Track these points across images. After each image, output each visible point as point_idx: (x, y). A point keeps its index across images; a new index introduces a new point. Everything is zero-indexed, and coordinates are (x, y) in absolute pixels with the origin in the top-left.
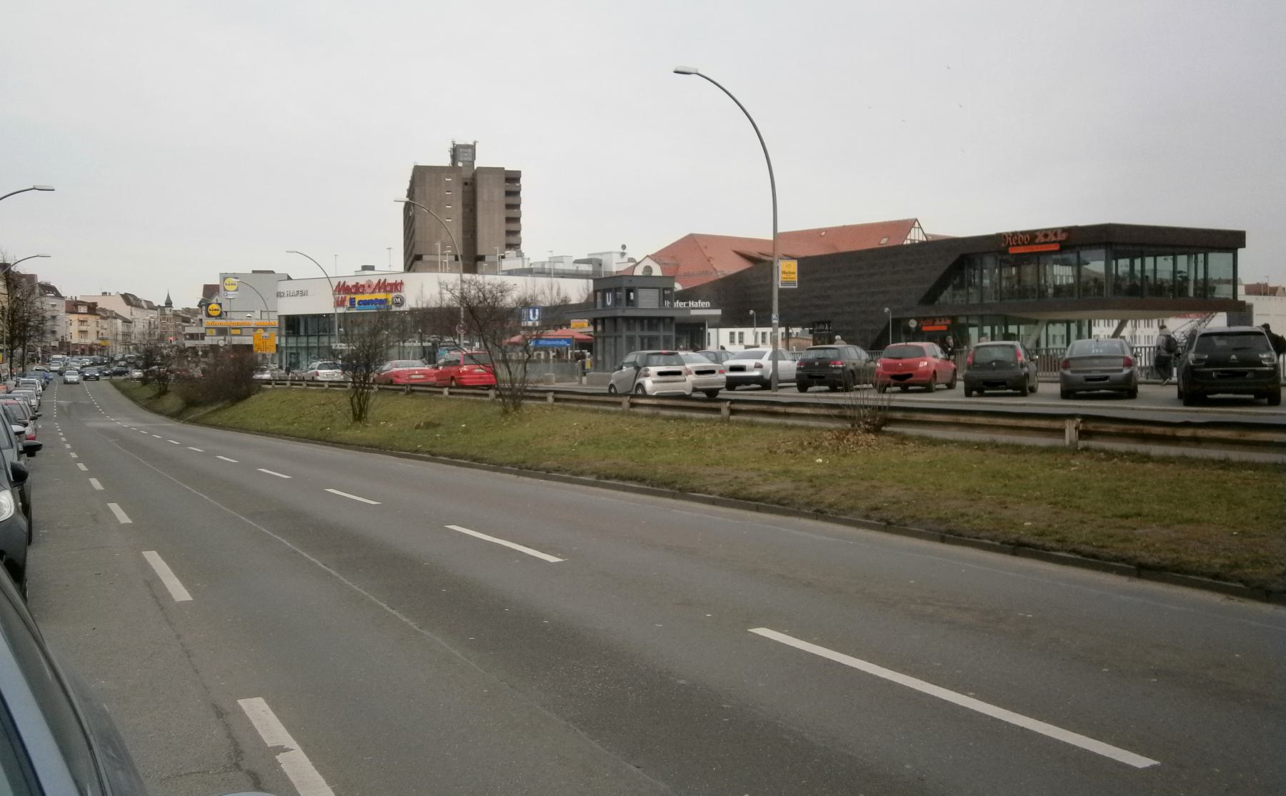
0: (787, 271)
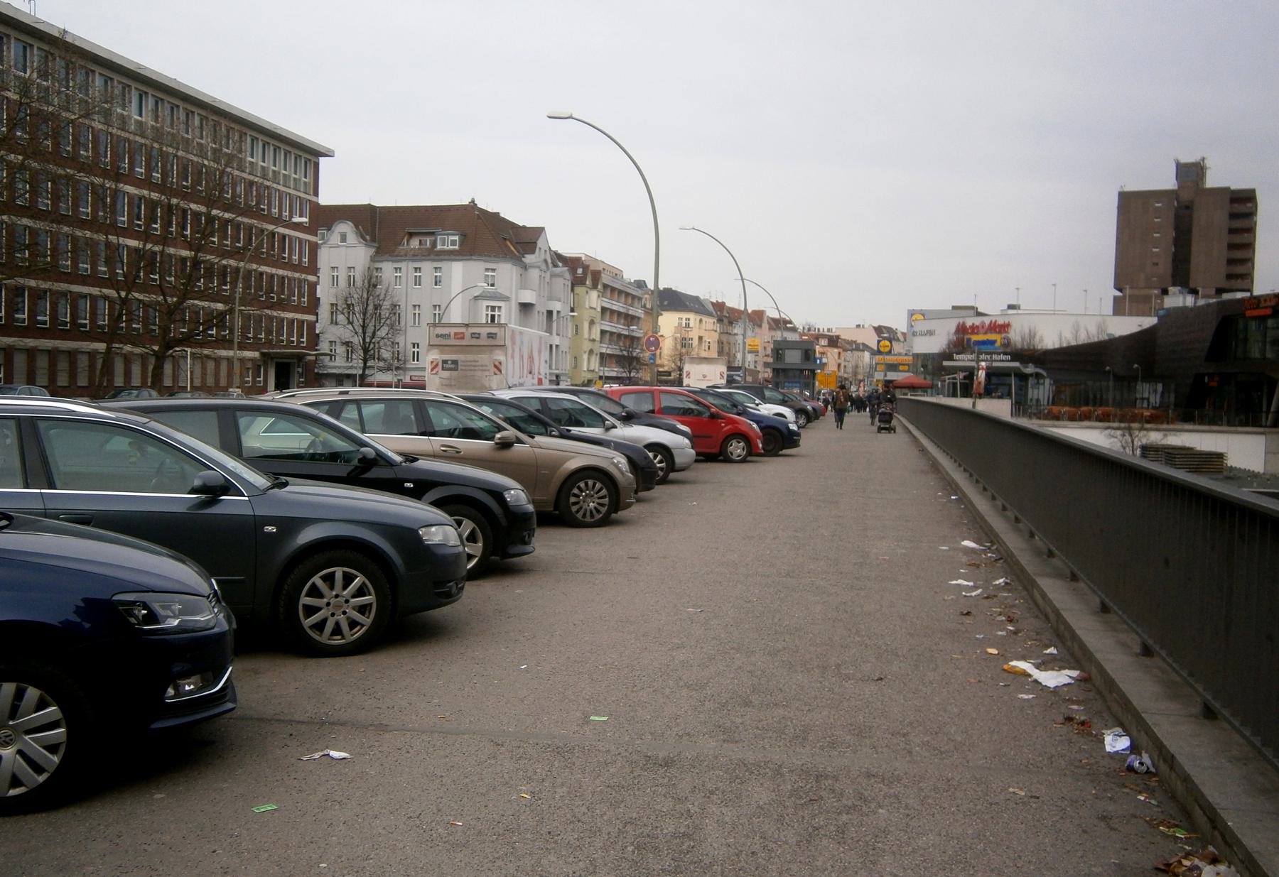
0: (752, 344)
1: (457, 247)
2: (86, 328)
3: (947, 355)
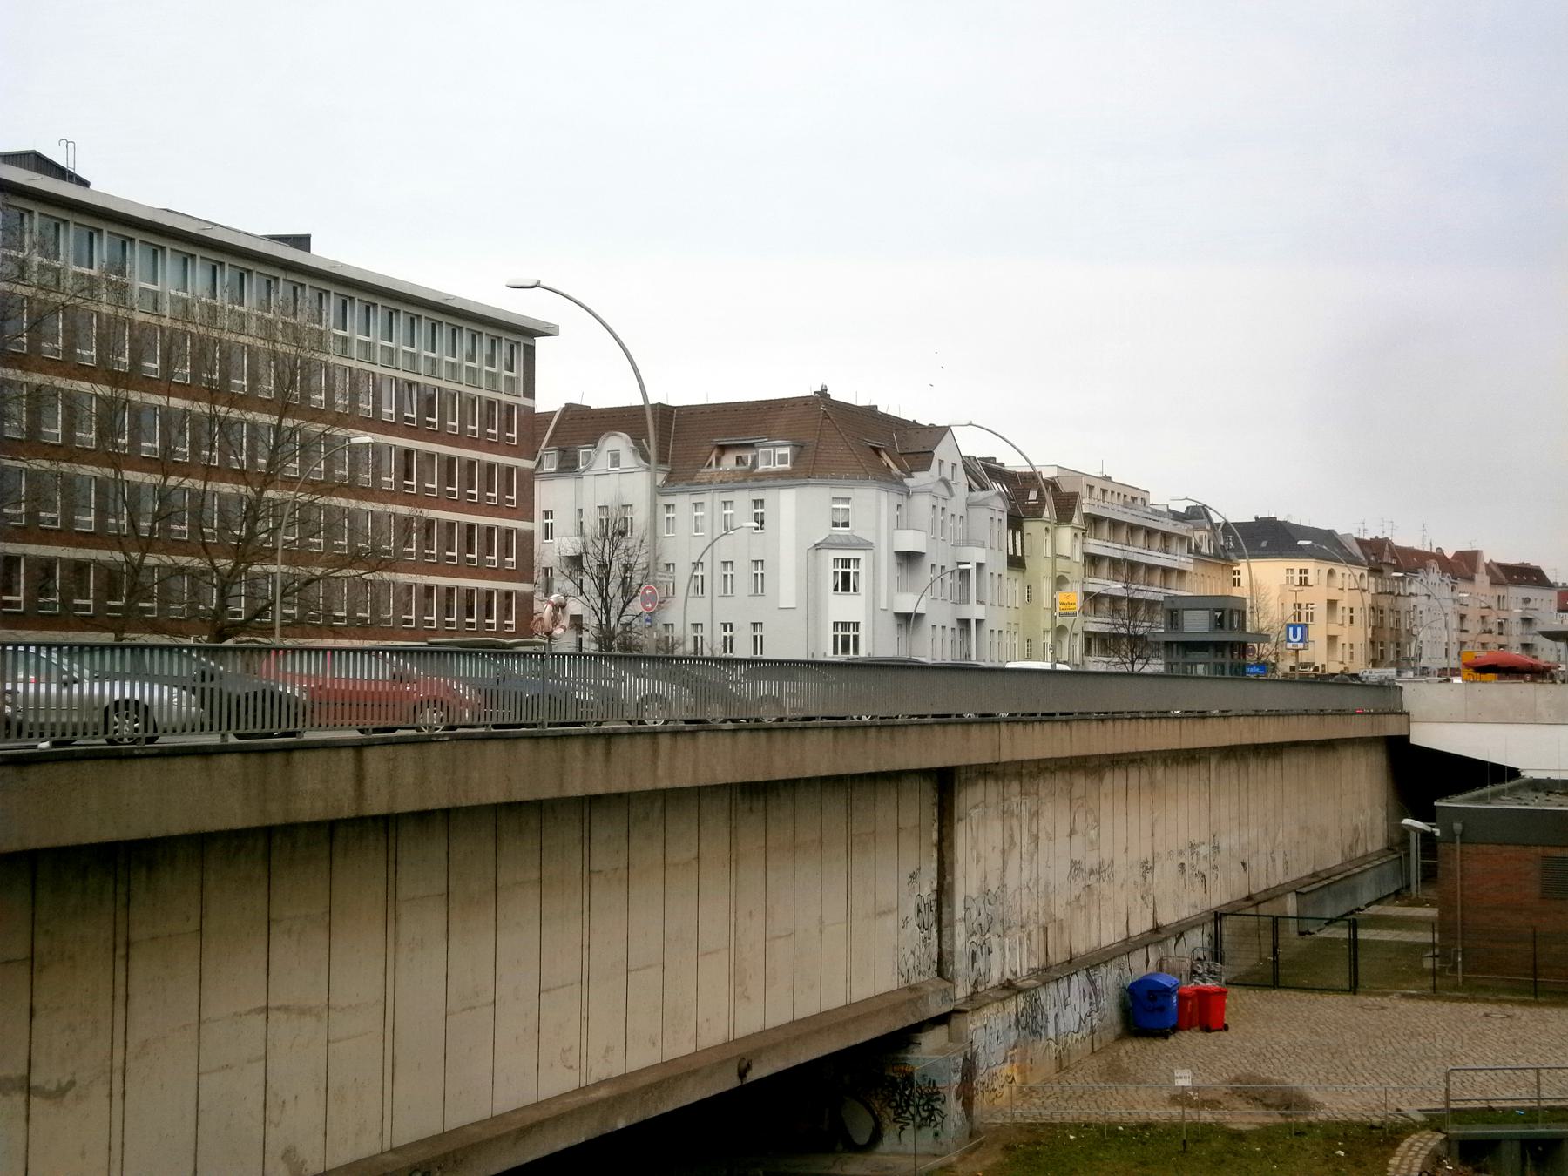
1: (788, 466)
2: (89, 611)
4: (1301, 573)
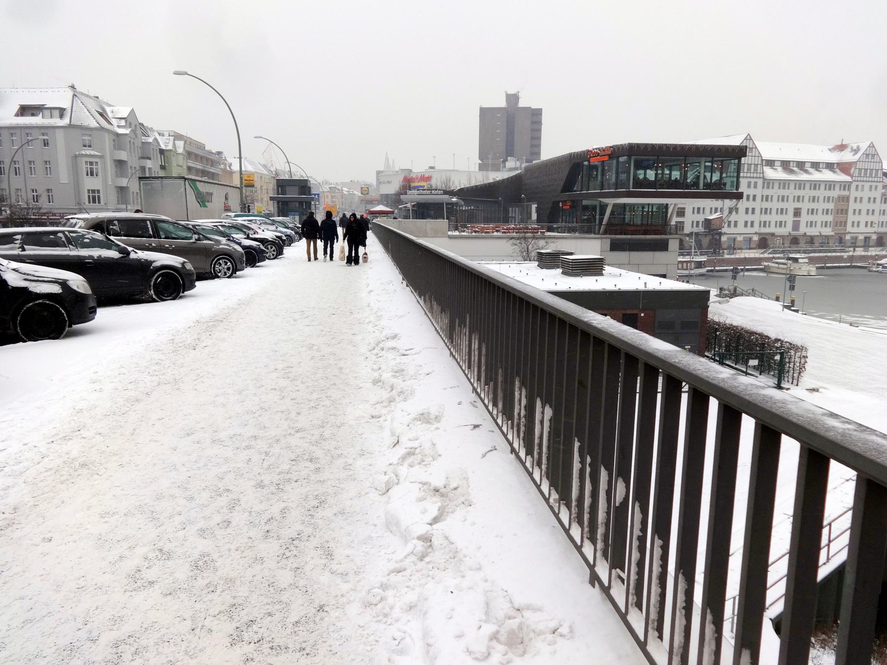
0: (248, 179)
3: (398, 194)
4: (89, 192)
